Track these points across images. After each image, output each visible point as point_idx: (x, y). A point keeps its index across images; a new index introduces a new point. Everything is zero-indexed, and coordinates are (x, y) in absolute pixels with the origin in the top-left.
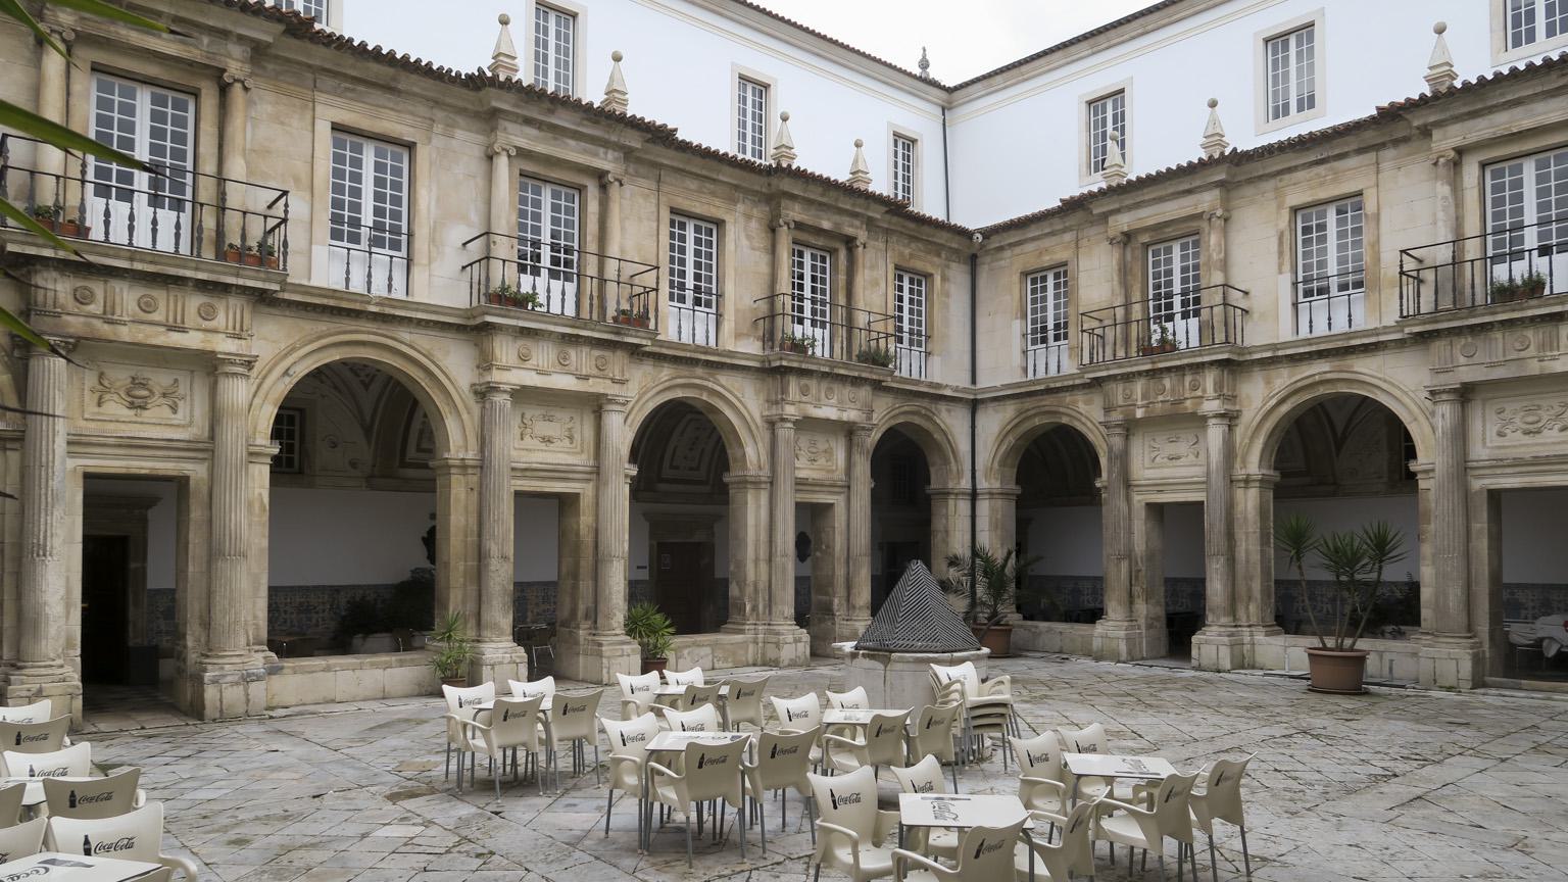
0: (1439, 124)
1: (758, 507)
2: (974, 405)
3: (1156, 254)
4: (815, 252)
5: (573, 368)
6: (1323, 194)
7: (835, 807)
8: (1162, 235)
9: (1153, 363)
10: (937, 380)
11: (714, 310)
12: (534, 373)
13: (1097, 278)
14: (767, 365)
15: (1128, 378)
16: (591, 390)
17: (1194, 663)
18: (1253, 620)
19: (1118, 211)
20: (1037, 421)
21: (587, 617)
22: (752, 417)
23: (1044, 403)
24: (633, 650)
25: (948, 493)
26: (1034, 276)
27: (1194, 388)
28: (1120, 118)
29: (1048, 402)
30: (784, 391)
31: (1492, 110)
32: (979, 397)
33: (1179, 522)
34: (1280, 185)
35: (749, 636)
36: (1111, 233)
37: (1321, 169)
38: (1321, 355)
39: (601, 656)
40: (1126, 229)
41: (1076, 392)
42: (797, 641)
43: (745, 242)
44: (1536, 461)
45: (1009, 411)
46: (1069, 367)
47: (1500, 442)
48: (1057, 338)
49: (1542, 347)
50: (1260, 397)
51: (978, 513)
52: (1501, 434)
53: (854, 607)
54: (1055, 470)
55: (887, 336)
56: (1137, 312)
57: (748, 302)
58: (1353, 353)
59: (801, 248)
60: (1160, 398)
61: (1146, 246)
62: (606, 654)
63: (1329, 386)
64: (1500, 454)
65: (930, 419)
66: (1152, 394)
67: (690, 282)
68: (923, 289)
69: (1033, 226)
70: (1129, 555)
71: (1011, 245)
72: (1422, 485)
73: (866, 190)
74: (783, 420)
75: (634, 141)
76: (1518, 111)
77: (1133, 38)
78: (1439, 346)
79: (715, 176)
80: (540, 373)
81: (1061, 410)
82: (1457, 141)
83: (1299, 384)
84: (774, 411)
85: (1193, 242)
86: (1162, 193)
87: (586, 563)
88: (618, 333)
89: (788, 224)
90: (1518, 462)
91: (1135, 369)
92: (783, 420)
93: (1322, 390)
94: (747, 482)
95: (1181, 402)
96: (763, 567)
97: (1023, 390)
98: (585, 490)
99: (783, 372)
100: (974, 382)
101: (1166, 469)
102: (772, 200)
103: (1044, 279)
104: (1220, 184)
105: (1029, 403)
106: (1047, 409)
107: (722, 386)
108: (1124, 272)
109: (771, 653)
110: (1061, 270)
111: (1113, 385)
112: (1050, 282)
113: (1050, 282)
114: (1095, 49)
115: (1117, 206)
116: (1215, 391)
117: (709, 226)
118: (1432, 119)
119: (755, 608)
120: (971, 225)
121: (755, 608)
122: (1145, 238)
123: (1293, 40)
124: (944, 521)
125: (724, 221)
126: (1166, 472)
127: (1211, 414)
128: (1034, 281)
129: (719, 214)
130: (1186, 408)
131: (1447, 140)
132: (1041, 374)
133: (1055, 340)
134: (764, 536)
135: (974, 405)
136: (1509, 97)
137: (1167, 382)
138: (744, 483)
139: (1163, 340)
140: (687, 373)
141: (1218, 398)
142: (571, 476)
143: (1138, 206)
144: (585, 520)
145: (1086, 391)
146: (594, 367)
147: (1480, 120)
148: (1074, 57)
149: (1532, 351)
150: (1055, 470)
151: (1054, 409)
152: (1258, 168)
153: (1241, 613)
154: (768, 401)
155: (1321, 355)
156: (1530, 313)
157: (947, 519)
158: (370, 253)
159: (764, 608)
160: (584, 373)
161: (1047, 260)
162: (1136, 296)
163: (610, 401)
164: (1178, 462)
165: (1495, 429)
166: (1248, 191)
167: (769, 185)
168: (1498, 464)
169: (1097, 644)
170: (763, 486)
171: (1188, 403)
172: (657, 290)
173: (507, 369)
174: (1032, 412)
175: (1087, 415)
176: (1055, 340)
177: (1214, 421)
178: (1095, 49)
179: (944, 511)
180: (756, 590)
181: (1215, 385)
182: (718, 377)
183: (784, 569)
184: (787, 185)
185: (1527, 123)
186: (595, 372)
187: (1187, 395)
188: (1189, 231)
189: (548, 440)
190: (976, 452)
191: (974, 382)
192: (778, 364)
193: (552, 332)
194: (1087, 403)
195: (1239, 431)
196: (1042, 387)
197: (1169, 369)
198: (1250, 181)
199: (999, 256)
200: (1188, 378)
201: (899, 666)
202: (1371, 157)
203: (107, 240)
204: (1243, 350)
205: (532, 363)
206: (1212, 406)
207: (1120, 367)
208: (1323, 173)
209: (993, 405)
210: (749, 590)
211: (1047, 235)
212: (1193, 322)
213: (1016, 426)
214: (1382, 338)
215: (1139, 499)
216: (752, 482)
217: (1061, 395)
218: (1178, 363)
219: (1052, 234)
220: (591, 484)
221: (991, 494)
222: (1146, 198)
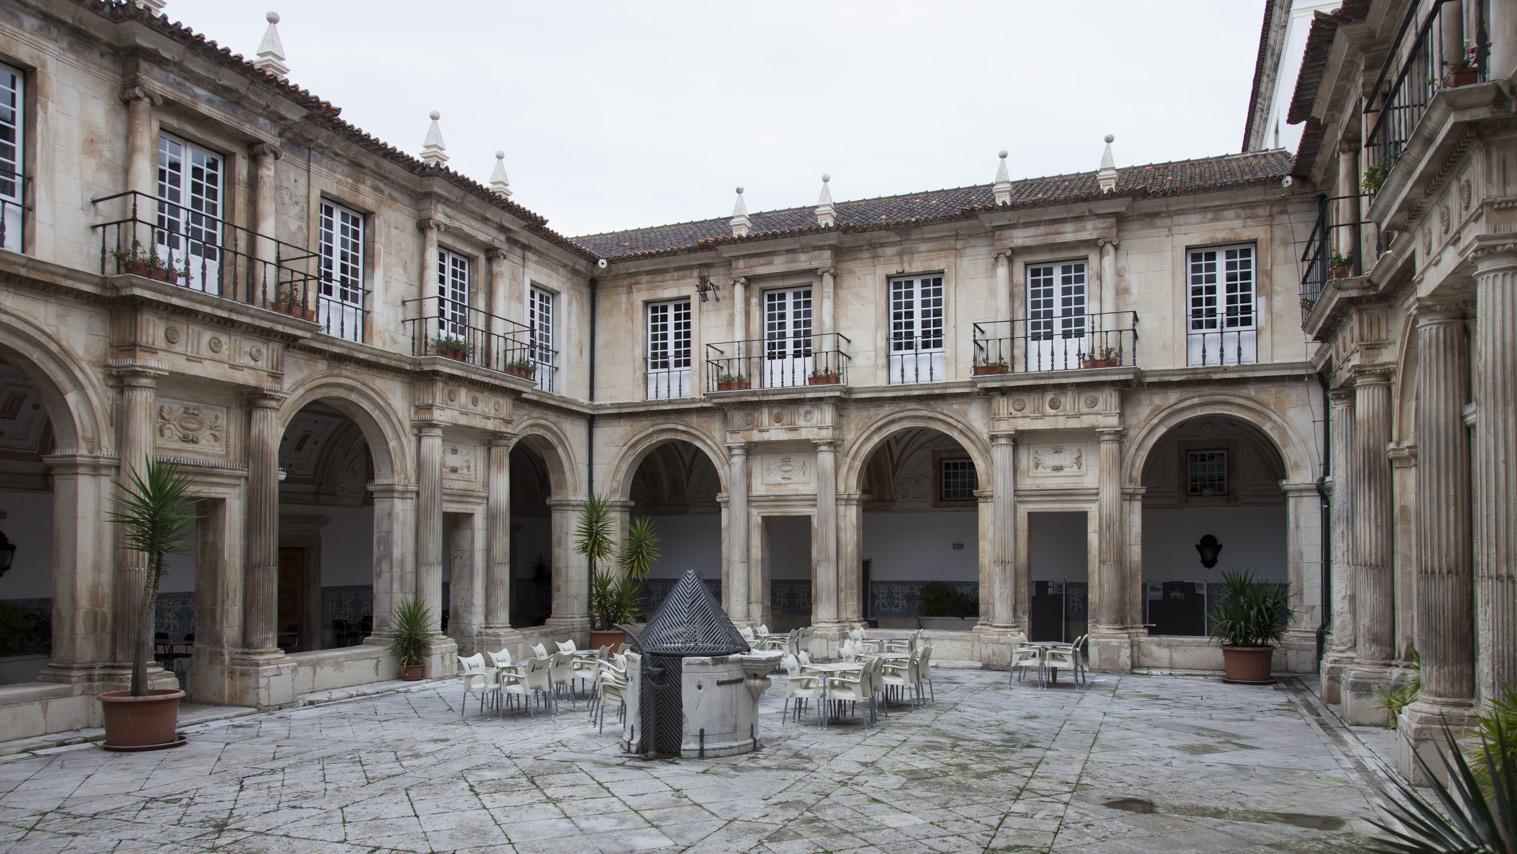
4: (456, 257)
10: (564, 393)
11: (360, 306)
26: (656, 308)
45: (645, 427)
46: (689, 392)
48: (678, 364)
54: (672, 486)
55: (306, 278)
56: (756, 352)
59: (330, 204)
67: (336, 273)
68: (466, 272)
73: (506, 200)
75: (294, 114)
89: (438, 226)
99: (431, 377)
100: (592, 397)
102: (421, 198)
113: (917, 288)
117: (357, 215)
133: (676, 366)
135: (591, 421)
150: (672, 486)
163: (265, 397)
164: (1062, 473)
172: (292, 271)
173: (153, 351)
176: (676, 366)
190: (598, 469)
191: (592, 397)
203: (204, 290)
220: (238, 489)
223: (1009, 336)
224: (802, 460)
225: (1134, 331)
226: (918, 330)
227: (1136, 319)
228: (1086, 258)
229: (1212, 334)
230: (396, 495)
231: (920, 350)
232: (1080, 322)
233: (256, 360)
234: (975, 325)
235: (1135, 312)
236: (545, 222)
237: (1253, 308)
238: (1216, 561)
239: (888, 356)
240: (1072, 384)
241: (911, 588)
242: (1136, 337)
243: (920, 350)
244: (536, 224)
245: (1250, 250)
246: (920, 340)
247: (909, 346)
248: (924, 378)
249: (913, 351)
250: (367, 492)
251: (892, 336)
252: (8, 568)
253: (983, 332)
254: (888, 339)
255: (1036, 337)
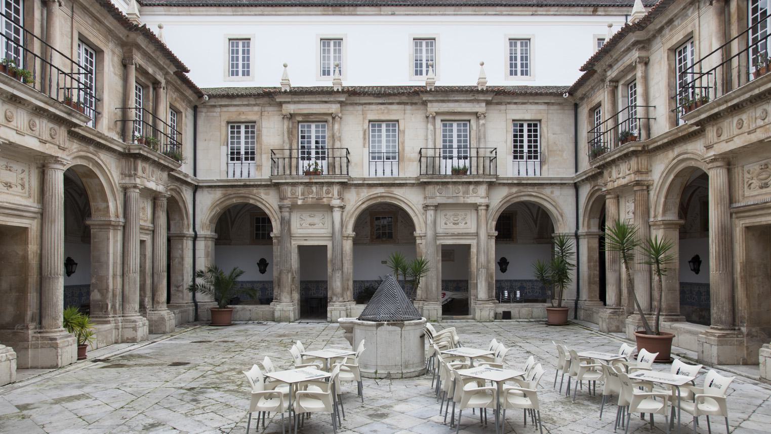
0: (431, 101)
1: (115, 242)
2: (196, 188)
3: (303, 127)
5: (37, 134)
6: (383, 118)
7: (710, 386)
8: (308, 118)
9: (310, 179)
12: (15, 132)
13: (272, 132)
14: (127, 151)
15: (294, 184)
16: (47, 152)
17: (329, 319)
18: (349, 299)
19: (289, 102)
20: (234, 201)
21: (33, 320)
22: (114, 180)
23: (240, 192)
24: (74, 341)
25: (184, 236)
26: (234, 126)
27: (328, 193)
28: (247, 52)
29: (243, 191)
30: (136, 169)
31: (449, 101)
32: (200, 184)
33: (313, 256)
34: (364, 109)
35: (112, 325)
36: (284, 112)
37: (382, 107)
38: (381, 185)
39: (56, 347)
40: (292, 112)
41: (259, 188)
42: (144, 325)
43: (112, 69)
44: (459, 235)
45: (218, 194)
47: (445, 226)
49: (464, 193)
50: (356, 201)
51: (197, 247)
52: (446, 224)
53: (158, 303)
57: (113, 108)
58: (394, 186)
60: (311, 196)
61: (299, 122)
62: (60, 345)
63: (382, 198)
64: (447, 231)
65: (179, 194)
66: (306, 193)
69: (238, 99)
70: (290, 271)
71: (221, 106)
72: (418, 241)
74: (135, 187)
76: (457, 104)
77: (256, 15)
78: (430, 189)
79: (102, 19)
80: (18, 133)
81: (251, 196)
82: (436, 110)
83: (372, 197)
84: (127, 181)
85: (307, 125)
86: (314, 99)
87: (33, 278)
88: (69, 114)
90: (453, 235)
91: (300, 181)
92: (135, 187)
93: (379, 200)
94: (110, 225)
95: (321, 199)
96: (119, 280)
97: (229, 184)
98: (32, 225)
100: (195, 175)
101: (308, 229)
103: (239, 127)
104: (341, 103)
105: (230, 191)
106: (242, 195)
107: (102, 160)
108: (290, 133)
109: (129, 334)
110: (251, 126)
111: (286, 187)
112: (243, 129)
113: (243, 129)
114: (234, 13)
115: (290, 100)
116: (338, 196)
118: (430, 99)
119: (114, 306)
120: (200, 85)
121: (114, 306)
122: (300, 119)
123: (332, 43)
124: (180, 252)
125: (102, 51)
126: (309, 231)
127: (337, 206)
128: (232, 127)
129: (101, 45)
130: (324, 202)
131: (433, 108)
132: (238, 176)
134: (119, 261)
135: (196, 188)
136: (456, 98)
137: (314, 189)
138: (108, 225)
139: (316, 170)
140: (85, 149)
141: (339, 199)
142: (25, 214)
143: (299, 102)
144: (33, 248)
145: (266, 188)
146: (49, 136)
147: (444, 104)
148: (223, 13)
149: (461, 194)
151: (247, 195)
152: (357, 99)
153: (345, 296)
154: (122, 174)
155: (381, 185)
156: (463, 180)
157: (183, 251)
158: (628, 107)
159: (120, 305)
160: (44, 138)
161: (243, 118)
162: (295, 146)
164: (314, 227)
165: (444, 222)
166: (350, 108)
167: (128, 36)
168: (447, 235)
169: (277, 314)
170: (119, 228)
171: (325, 200)
172: (496, 157)
174: (234, 195)
175: (269, 201)
177: (337, 209)
178: (234, 13)
179: (180, 246)
180: (114, 295)
181: (338, 192)
182: (99, 154)
183: (135, 282)
184: (141, 40)
185: (460, 110)
186: (49, 139)
187: (324, 196)
188: (322, 119)
189: (8, 185)
192: (137, 151)
193: (31, 103)
194: (266, 194)
195: (345, 214)
196: (242, 183)
197: (316, 183)
198: (352, 104)
199: (212, 110)
200: (325, 188)
201: (408, 328)
202: (402, 107)
204: (351, 179)
205: (13, 124)
206: (336, 202)
207: (293, 179)
208: (383, 109)
209: (207, 189)
210: (110, 295)
211: (244, 105)
212: (325, 163)
213: (221, 203)
214: (408, 182)
215: (295, 243)
216: (113, 226)
217: (251, 189)
218: (323, 181)
219: (247, 105)
220: (36, 220)
221: (205, 238)
222: (305, 100)
223: (476, 156)
224: (321, 215)
225: (347, 158)
226: (526, 149)
227: (348, 153)
228: (469, 121)
229: (522, 163)
230: (661, 223)
231: (244, 161)
232: (323, 153)
233: (53, 138)
234: (496, 149)
235: (347, 149)
236: (188, 71)
237: (539, 151)
238: (265, 271)
239: (227, 164)
240: (326, 182)
241: (522, 284)
242: (348, 161)
243: (385, 160)
244: (181, 70)
245: (395, 124)
246: (244, 156)
247: (238, 159)
248: (245, 176)
249: (240, 162)
250: (686, 218)
251: (229, 153)
252: (74, 272)
253: (275, 154)
254: (228, 155)
255: (303, 158)
